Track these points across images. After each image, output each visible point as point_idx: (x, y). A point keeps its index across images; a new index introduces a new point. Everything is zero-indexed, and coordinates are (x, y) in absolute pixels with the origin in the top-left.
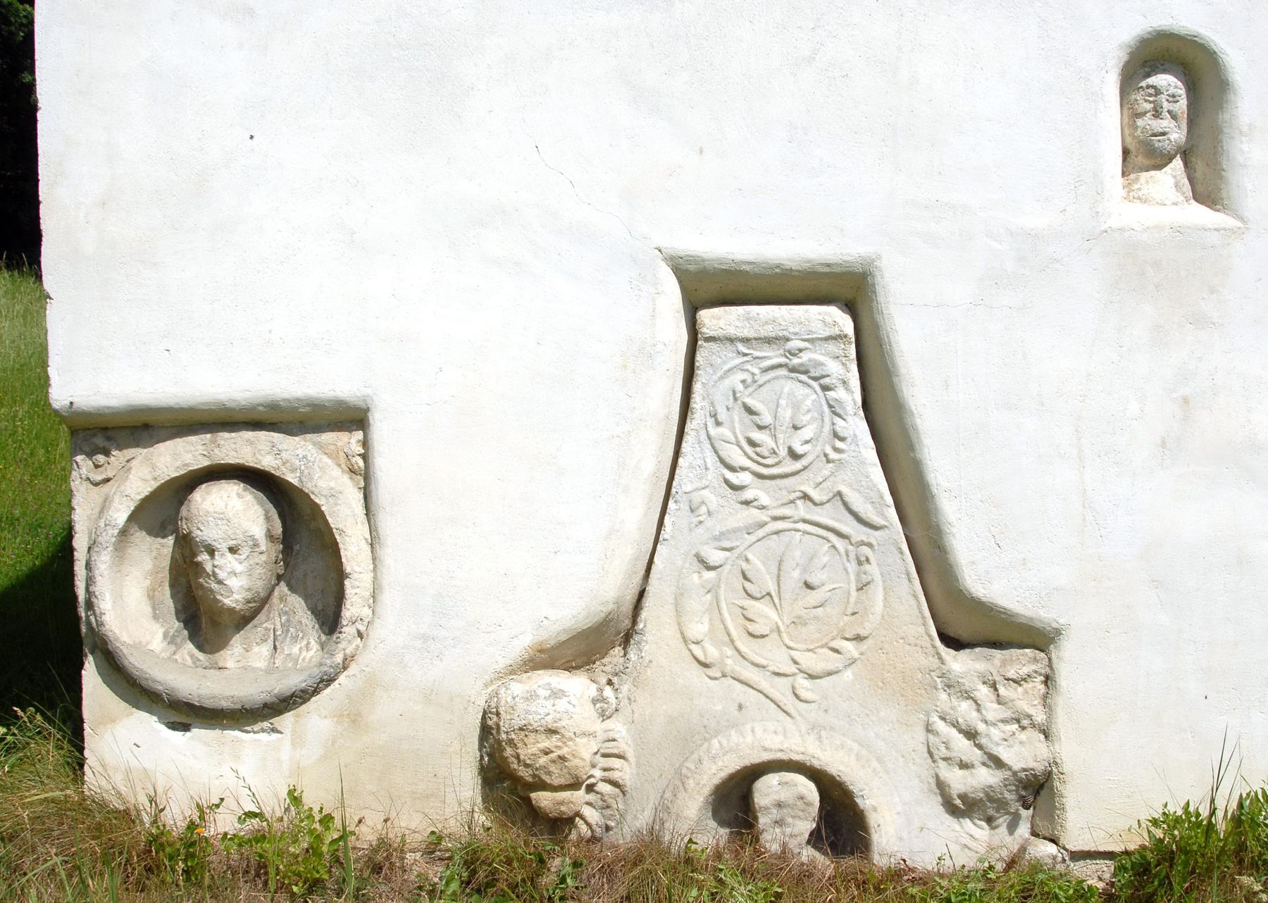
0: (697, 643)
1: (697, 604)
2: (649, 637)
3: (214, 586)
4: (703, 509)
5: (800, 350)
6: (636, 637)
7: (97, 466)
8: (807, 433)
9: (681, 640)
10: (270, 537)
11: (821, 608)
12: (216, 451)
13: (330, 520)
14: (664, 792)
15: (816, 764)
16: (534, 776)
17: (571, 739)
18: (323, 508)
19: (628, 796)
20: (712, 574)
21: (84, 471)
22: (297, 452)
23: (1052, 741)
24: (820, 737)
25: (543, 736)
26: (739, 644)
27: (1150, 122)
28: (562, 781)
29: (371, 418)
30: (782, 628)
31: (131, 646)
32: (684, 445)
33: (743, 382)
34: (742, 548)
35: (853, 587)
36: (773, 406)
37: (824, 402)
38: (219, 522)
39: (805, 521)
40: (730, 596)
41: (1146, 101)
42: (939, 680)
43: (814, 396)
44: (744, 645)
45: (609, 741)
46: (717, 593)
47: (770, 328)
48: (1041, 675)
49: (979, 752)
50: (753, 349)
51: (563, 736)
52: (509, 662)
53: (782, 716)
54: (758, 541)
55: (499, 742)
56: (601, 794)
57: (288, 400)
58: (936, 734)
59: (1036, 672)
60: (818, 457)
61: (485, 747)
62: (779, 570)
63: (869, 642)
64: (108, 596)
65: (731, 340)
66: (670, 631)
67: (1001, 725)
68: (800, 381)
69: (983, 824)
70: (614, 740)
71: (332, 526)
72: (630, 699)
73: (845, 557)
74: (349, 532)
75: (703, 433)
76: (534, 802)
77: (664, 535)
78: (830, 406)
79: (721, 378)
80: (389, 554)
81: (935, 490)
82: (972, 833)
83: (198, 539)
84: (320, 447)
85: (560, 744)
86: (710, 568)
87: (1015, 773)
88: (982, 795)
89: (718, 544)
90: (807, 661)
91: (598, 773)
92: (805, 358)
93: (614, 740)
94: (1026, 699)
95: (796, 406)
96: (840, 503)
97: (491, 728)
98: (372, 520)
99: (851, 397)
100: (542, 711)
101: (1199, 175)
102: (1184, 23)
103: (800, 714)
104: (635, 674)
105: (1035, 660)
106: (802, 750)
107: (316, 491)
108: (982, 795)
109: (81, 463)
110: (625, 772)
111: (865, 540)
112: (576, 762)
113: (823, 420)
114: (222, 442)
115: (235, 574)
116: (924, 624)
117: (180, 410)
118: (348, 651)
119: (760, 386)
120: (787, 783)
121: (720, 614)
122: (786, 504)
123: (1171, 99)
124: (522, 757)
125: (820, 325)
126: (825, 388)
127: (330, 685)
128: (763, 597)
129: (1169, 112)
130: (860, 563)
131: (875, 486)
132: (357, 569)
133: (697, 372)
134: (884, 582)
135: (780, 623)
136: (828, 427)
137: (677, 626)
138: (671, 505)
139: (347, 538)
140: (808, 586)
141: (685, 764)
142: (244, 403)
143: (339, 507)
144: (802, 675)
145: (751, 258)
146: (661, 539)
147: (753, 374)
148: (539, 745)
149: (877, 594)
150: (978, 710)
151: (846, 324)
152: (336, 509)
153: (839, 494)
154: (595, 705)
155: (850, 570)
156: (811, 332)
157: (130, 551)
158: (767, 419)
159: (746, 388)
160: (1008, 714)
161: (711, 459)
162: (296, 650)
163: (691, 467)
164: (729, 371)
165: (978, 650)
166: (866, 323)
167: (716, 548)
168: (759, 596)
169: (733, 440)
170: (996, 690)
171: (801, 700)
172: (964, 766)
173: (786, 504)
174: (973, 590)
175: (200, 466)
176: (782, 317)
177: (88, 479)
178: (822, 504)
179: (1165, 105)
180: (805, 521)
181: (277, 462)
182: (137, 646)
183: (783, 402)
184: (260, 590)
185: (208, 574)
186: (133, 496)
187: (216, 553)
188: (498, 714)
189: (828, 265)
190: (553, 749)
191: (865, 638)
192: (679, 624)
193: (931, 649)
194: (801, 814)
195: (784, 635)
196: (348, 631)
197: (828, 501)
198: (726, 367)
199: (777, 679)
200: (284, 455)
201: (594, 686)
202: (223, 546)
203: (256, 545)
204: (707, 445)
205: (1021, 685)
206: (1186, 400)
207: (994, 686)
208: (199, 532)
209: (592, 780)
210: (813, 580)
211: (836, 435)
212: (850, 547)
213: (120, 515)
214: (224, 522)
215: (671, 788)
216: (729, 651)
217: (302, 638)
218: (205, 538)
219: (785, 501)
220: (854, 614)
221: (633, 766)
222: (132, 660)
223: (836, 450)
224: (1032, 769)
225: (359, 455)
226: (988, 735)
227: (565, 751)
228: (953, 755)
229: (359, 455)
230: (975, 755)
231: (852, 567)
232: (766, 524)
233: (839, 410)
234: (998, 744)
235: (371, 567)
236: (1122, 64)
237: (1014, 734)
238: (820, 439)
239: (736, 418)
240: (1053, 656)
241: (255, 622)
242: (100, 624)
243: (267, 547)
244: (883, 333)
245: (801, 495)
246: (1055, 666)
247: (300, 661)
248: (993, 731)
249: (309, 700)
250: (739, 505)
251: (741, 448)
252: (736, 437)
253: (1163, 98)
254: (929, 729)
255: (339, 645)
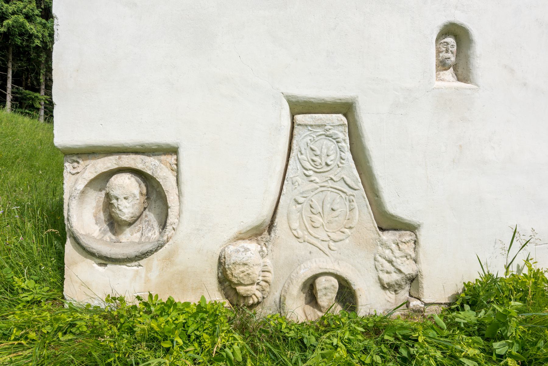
0: (295, 230)
1: (295, 216)
2: (278, 228)
3: (118, 212)
4: (297, 184)
5: (330, 129)
6: (274, 228)
7: (74, 168)
8: (332, 157)
9: (289, 229)
10: (141, 194)
11: (337, 218)
12: (120, 162)
13: (163, 187)
14: (284, 284)
15: (338, 273)
16: (238, 281)
17: (252, 267)
18: (161, 183)
19: (271, 286)
20: (300, 206)
21: (68, 170)
22: (152, 163)
23: (418, 264)
24: (339, 263)
25: (242, 266)
26: (309, 230)
27: (444, 54)
28: (248, 283)
29: (179, 150)
30: (324, 225)
31: (85, 235)
32: (290, 161)
33: (310, 140)
34: (310, 197)
35: (348, 210)
36: (320, 148)
37: (337, 147)
38: (120, 188)
39: (331, 187)
40: (306, 213)
41: (443, 47)
42: (378, 242)
43: (334, 145)
44: (311, 230)
45: (265, 266)
46: (301, 212)
47: (320, 121)
48: (413, 240)
49: (393, 268)
50: (314, 129)
51: (249, 266)
52: (229, 238)
53: (325, 256)
54: (315, 194)
55: (225, 269)
56: (262, 286)
57: (148, 144)
58: (378, 261)
59: (411, 239)
60: (335, 166)
61: (220, 270)
62: (323, 204)
63: (354, 229)
64: (75, 216)
65: (306, 125)
66: (286, 226)
67: (400, 258)
68: (329, 140)
69: (393, 293)
70: (266, 266)
71: (164, 189)
72: (272, 251)
73: (345, 200)
74: (170, 191)
75: (296, 157)
76: (237, 291)
77: (283, 192)
78: (339, 148)
79: (303, 139)
80: (185, 199)
81: (376, 177)
82: (390, 296)
83: (112, 195)
84: (161, 161)
85: (248, 269)
86: (299, 204)
87: (406, 275)
88: (394, 283)
89: (302, 195)
90: (333, 236)
91: (261, 278)
92: (331, 132)
93: (266, 266)
94: (409, 249)
95: (328, 149)
96: (343, 181)
97: (222, 263)
98: (179, 187)
99: (346, 146)
100: (242, 257)
101: (460, 72)
102: (458, 20)
103: (331, 255)
104: (273, 242)
105: (411, 235)
106: (333, 268)
107: (158, 177)
108: (394, 283)
109: (67, 167)
110: (270, 277)
111: (352, 194)
112: (254, 275)
113: (337, 153)
114: (123, 159)
115: (126, 207)
116: (373, 223)
117: (102, 147)
118: (169, 235)
119: (316, 141)
120: (328, 280)
121: (303, 220)
122: (325, 182)
123: (452, 47)
124: (234, 274)
125: (336, 121)
126: (338, 142)
127: (162, 248)
128: (317, 214)
129: (451, 51)
130: (350, 202)
131: (355, 175)
132: (173, 205)
133: (294, 136)
134: (359, 208)
135: (323, 223)
136: (122, 252)
137: (288, 224)
138: (286, 182)
139: (170, 194)
140: (333, 210)
141: (292, 274)
142: (131, 144)
143: (167, 183)
144: (331, 241)
145: (314, 97)
146: (282, 193)
147: (314, 137)
148: (240, 270)
149: (356, 212)
150: (393, 253)
151: (344, 119)
152: (165, 183)
153: (343, 178)
154: (260, 253)
155: (347, 204)
156: (333, 123)
157: (86, 199)
158: (318, 152)
159: (311, 142)
160: (403, 254)
161: (299, 166)
162: (150, 234)
163: (292, 169)
164: (305, 136)
165: (390, 231)
166: (351, 120)
167: (301, 197)
168: (316, 213)
169: (307, 160)
170: (398, 246)
171: (331, 250)
172: (388, 273)
173: (325, 182)
174: (390, 211)
175: (114, 168)
176: (324, 118)
177: (70, 173)
178: (337, 182)
179: (450, 48)
180: (331, 187)
181: (144, 166)
182: (87, 235)
183: (324, 147)
184: (137, 213)
185: (116, 207)
186: (86, 178)
187: (119, 200)
188: (225, 258)
189: (340, 100)
190: (245, 271)
191: (353, 228)
192: (289, 223)
193: (376, 232)
194: (333, 291)
195: (325, 227)
196: (169, 228)
197: (339, 181)
198: (305, 135)
199: (323, 243)
200: (147, 164)
201: (259, 246)
202: (121, 197)
203: (135, 196)
204: (298, 162)
205: (406, 244)
206: (461, 146)
207: (398, 245)
208: (112, 192)
209: (259, 281)
210: (334, 208)
211: (341, 158)
212: (347, 196)
213: (81, 186)
214: (122, 188)
215: (287, 283)
216: (306, 233)
217: (153, 230)
218: (115, 194)
219: (324, 180)
220: (349, 219)
221: (273, 275)
222: (84, 240)
223: (341, 163)
224: (412, 274)
225: (175, 164)
226: (396, 262)
227: (249, 272)
228: (384, 269)
229: (175, 164)
230: (391, 269)
231: (347, 203)
232: (318, 188)
233: (342, 150)
234: (400, 265)
235: (179, 204)
236: (438, 33)
237: (405, 261)
238: (336, 160)
239: (308, 152)
240: (417, 234)
241: (135, 224)
242: (72, 227)
243: (140, 198)
244: (358, 123)
245: (330, 178)
246: (418, 237)
247: (151, 238)
248: (398, 260)
249: (153, 253)
250: (309, 182)
251: (309, 162)
252: (308, 159)
253: (449, 46)
254: (375, 260)
255: (166, 233)
